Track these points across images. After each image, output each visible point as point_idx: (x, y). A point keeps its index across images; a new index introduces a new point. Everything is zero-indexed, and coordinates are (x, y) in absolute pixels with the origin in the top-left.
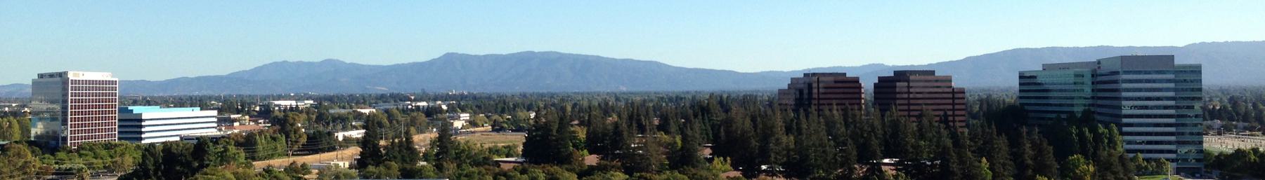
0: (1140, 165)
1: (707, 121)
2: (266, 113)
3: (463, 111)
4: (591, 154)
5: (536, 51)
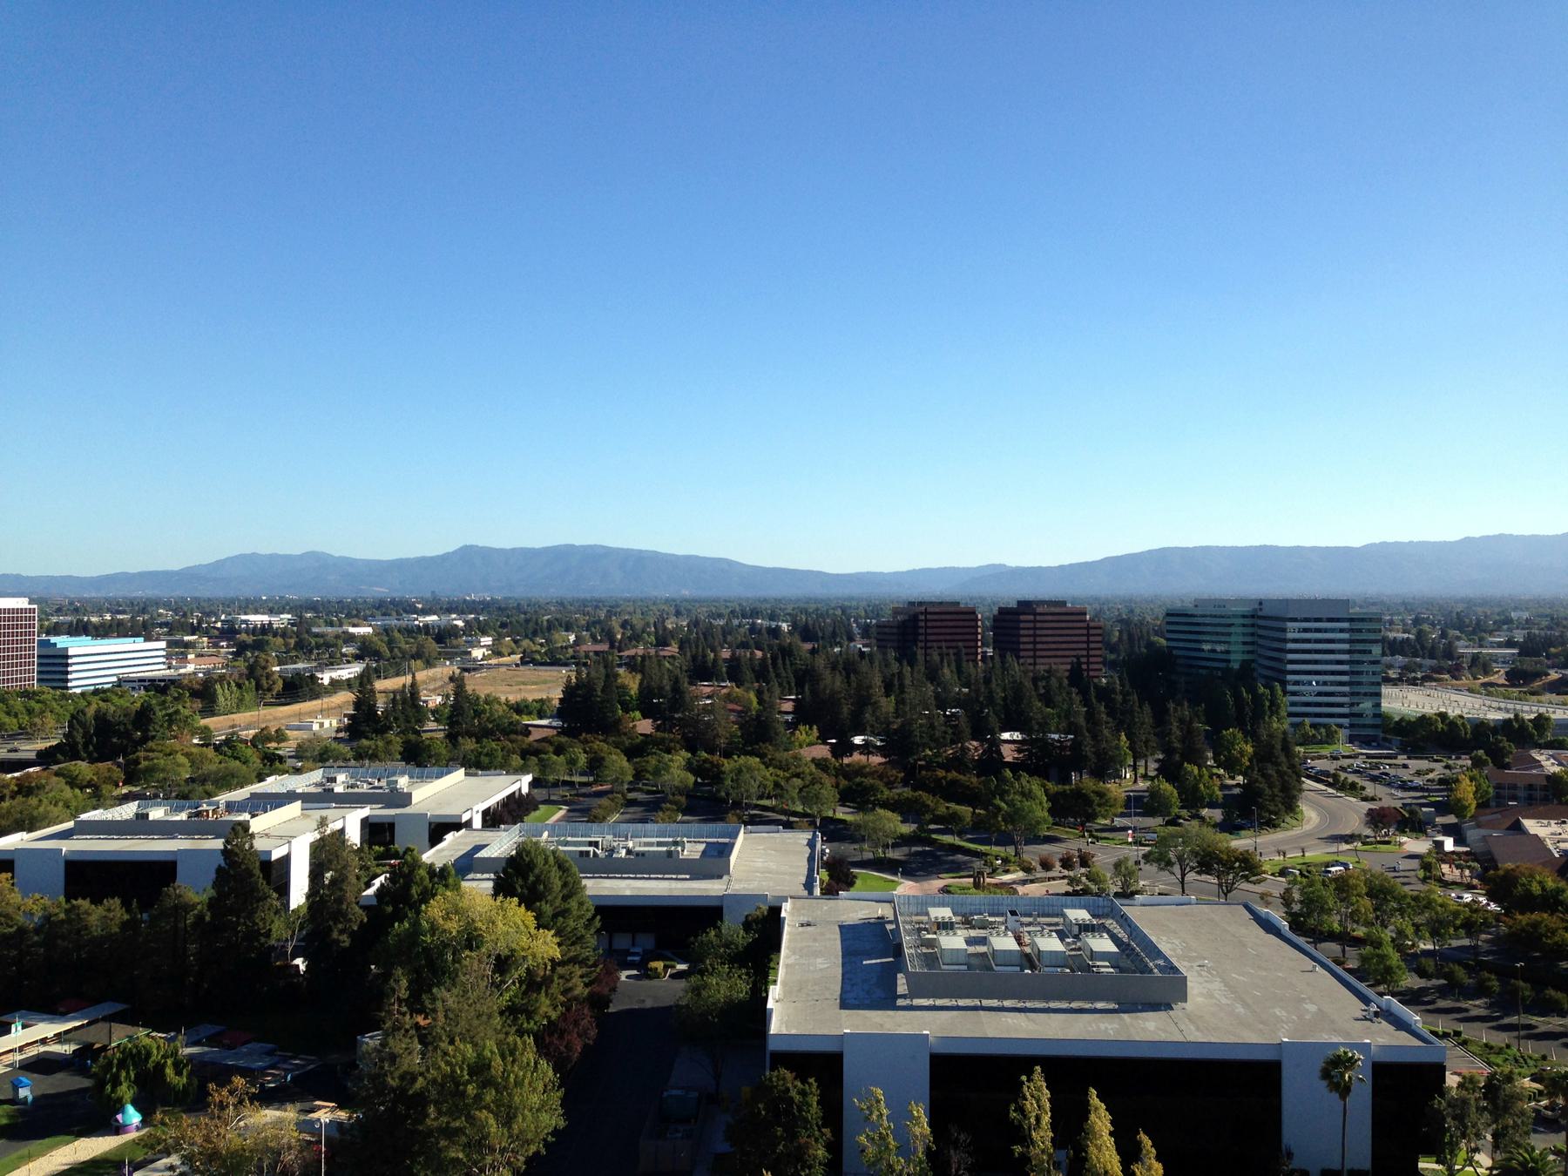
0: (1307, 733)
1: (788, 666)
2: (229, 632)
3: (484, 633)
4: (644, 718)
5: (577, 544)
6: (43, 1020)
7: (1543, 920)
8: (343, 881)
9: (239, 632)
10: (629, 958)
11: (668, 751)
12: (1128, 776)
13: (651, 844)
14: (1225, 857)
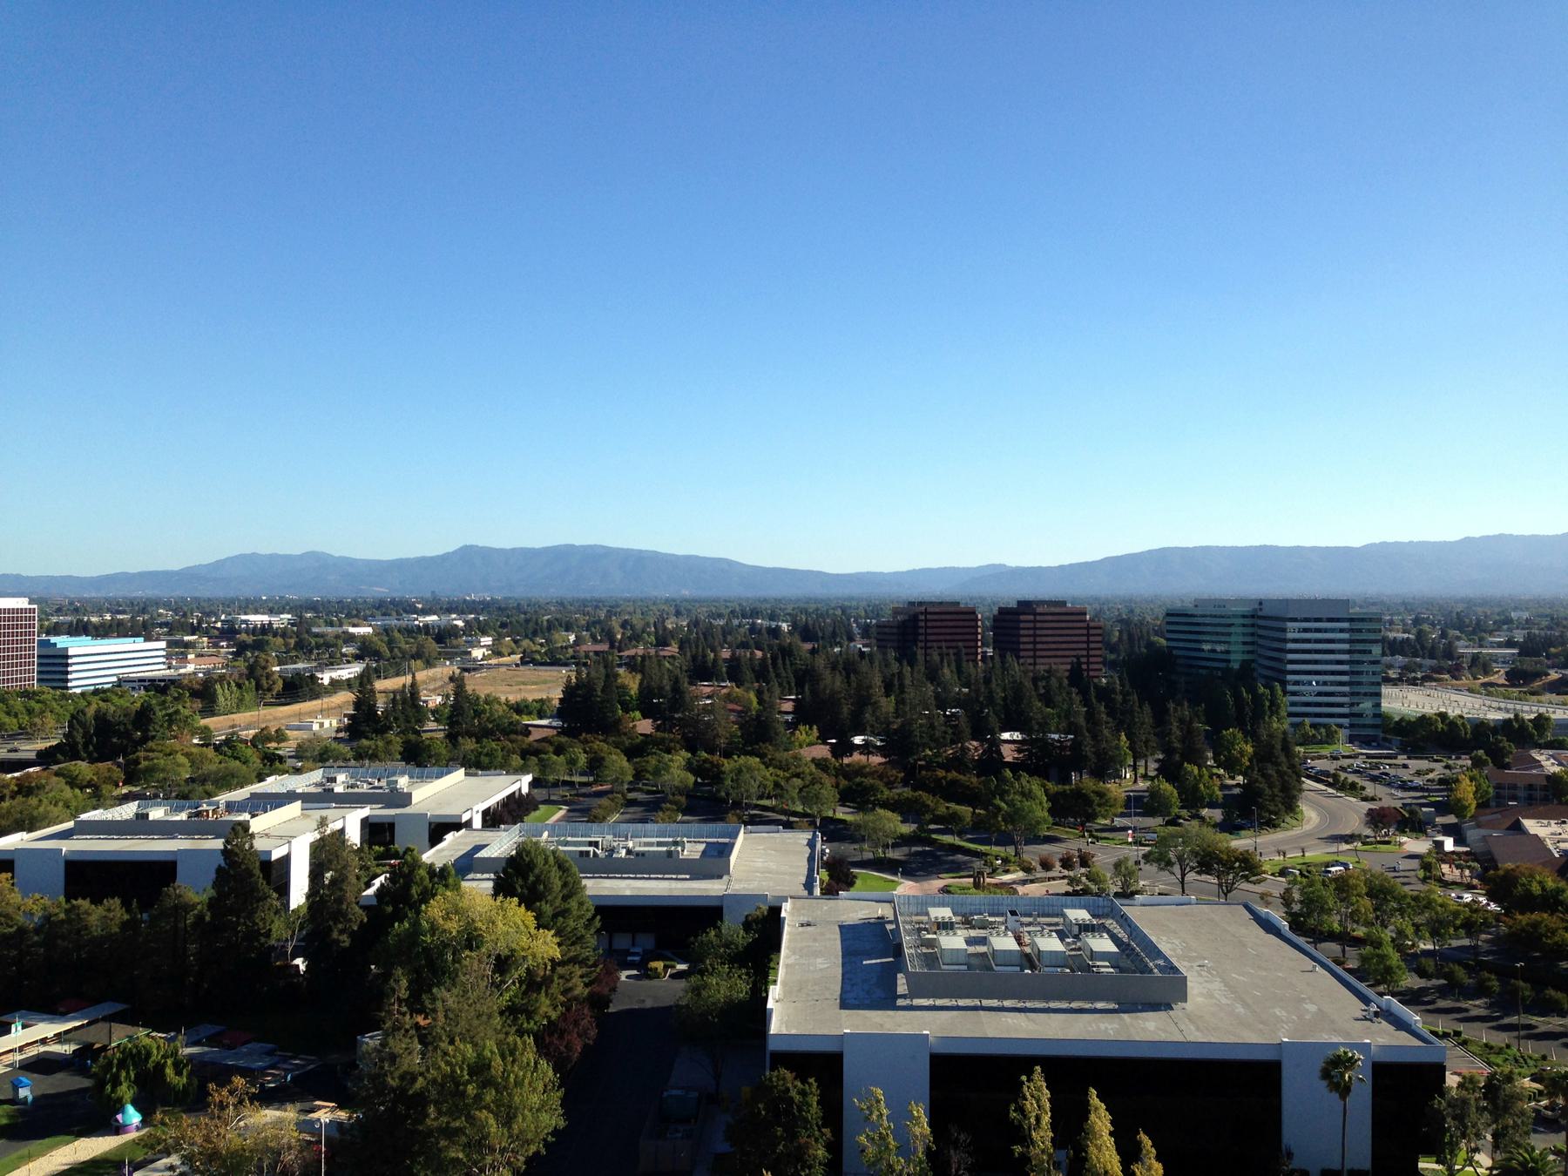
0: (1307, 733)
1: (788, 666)
2: (229, 632)
3: (484, 633)
4: (644, 718)
5: (577, 544)
6: (43, 1020)
7: (1543, 920)
8: (343, 881)
9: (239, 632)
10: (629, 958)
11: (668, 751)
12: (1128, 776)
13: (651, 844)
14: (1225, 857)
